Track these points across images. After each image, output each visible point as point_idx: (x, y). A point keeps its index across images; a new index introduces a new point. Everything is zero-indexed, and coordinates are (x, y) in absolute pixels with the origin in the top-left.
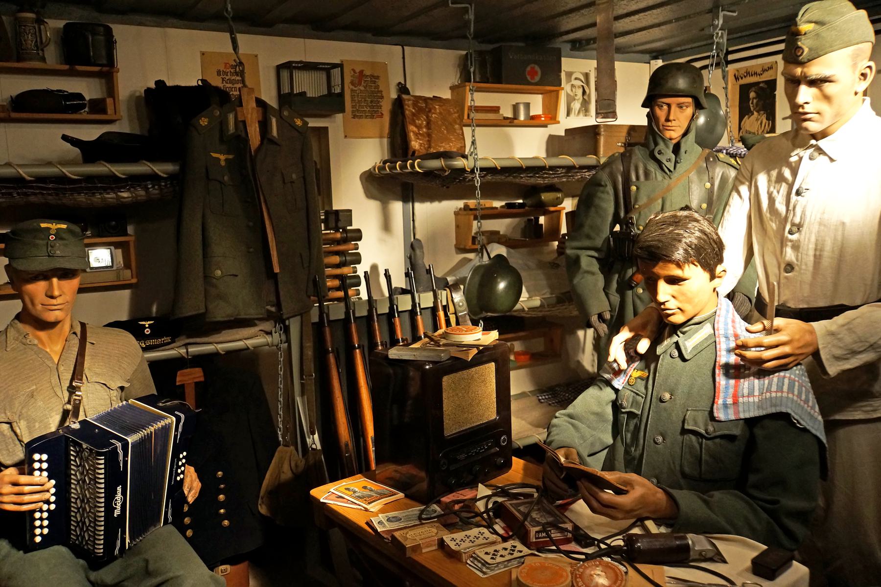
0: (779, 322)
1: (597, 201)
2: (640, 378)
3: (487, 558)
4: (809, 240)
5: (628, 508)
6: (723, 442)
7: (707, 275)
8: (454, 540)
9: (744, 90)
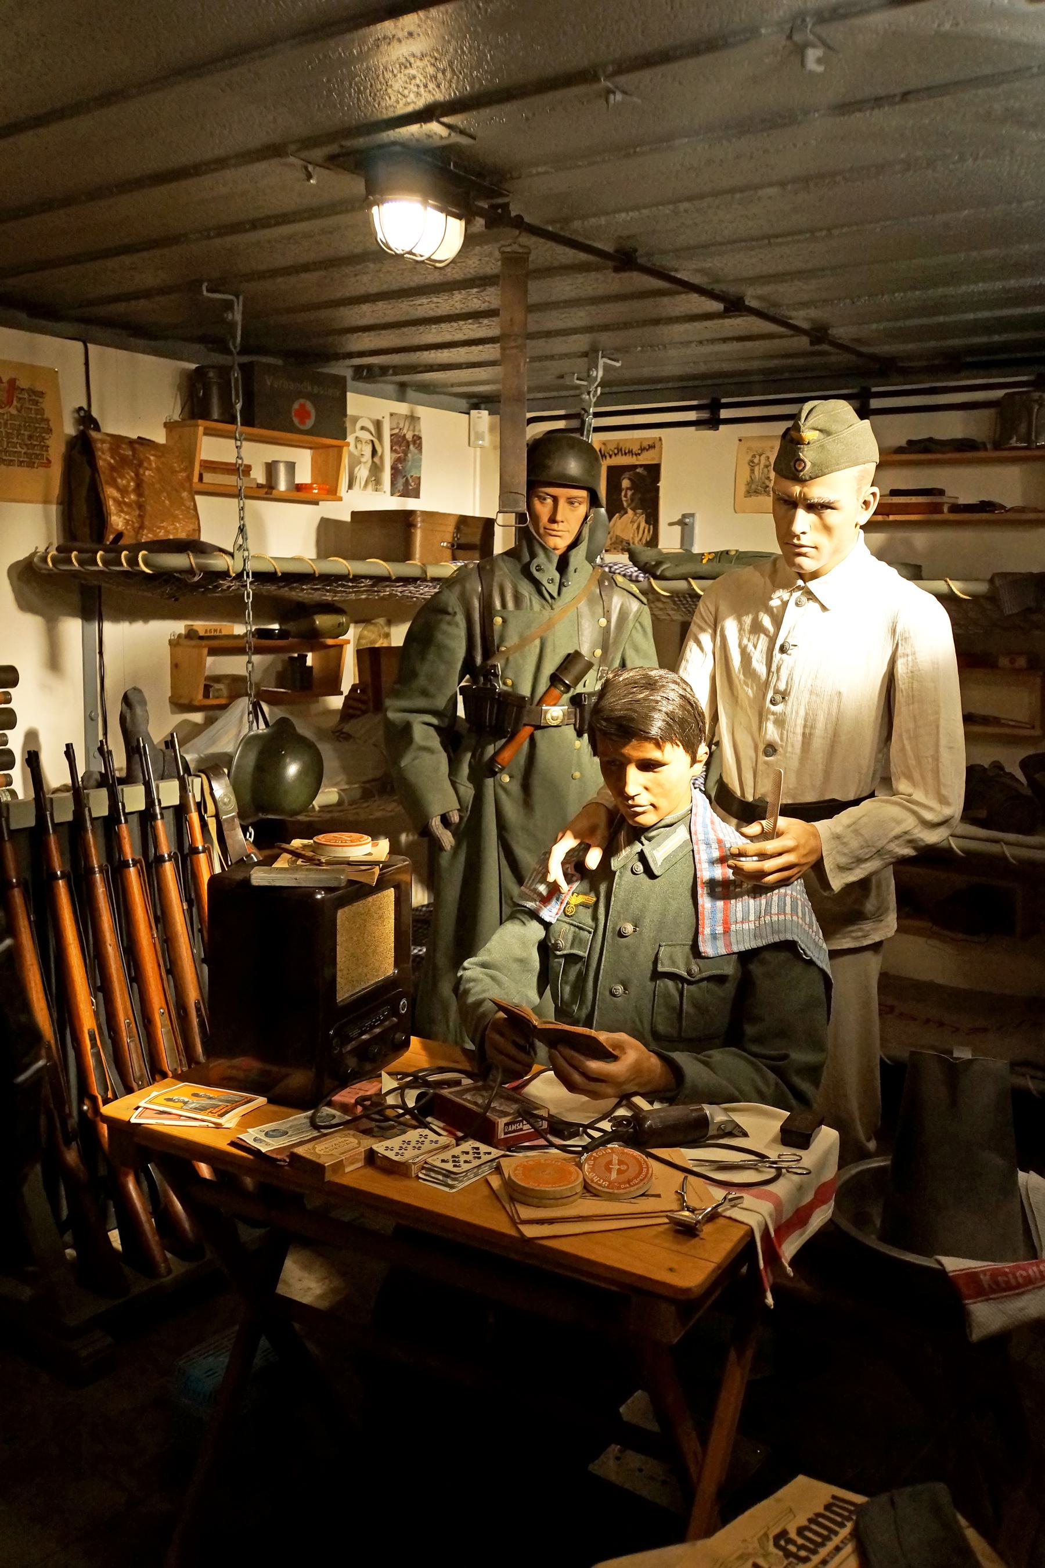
0: (783, 822)
1: (440, 637)
2: (585, 905)
3: (449, 1166)
4: (797, 713)
5: (622, 1079)
6: (712, 986)
7: (687, 759)
8: (388, 1148)
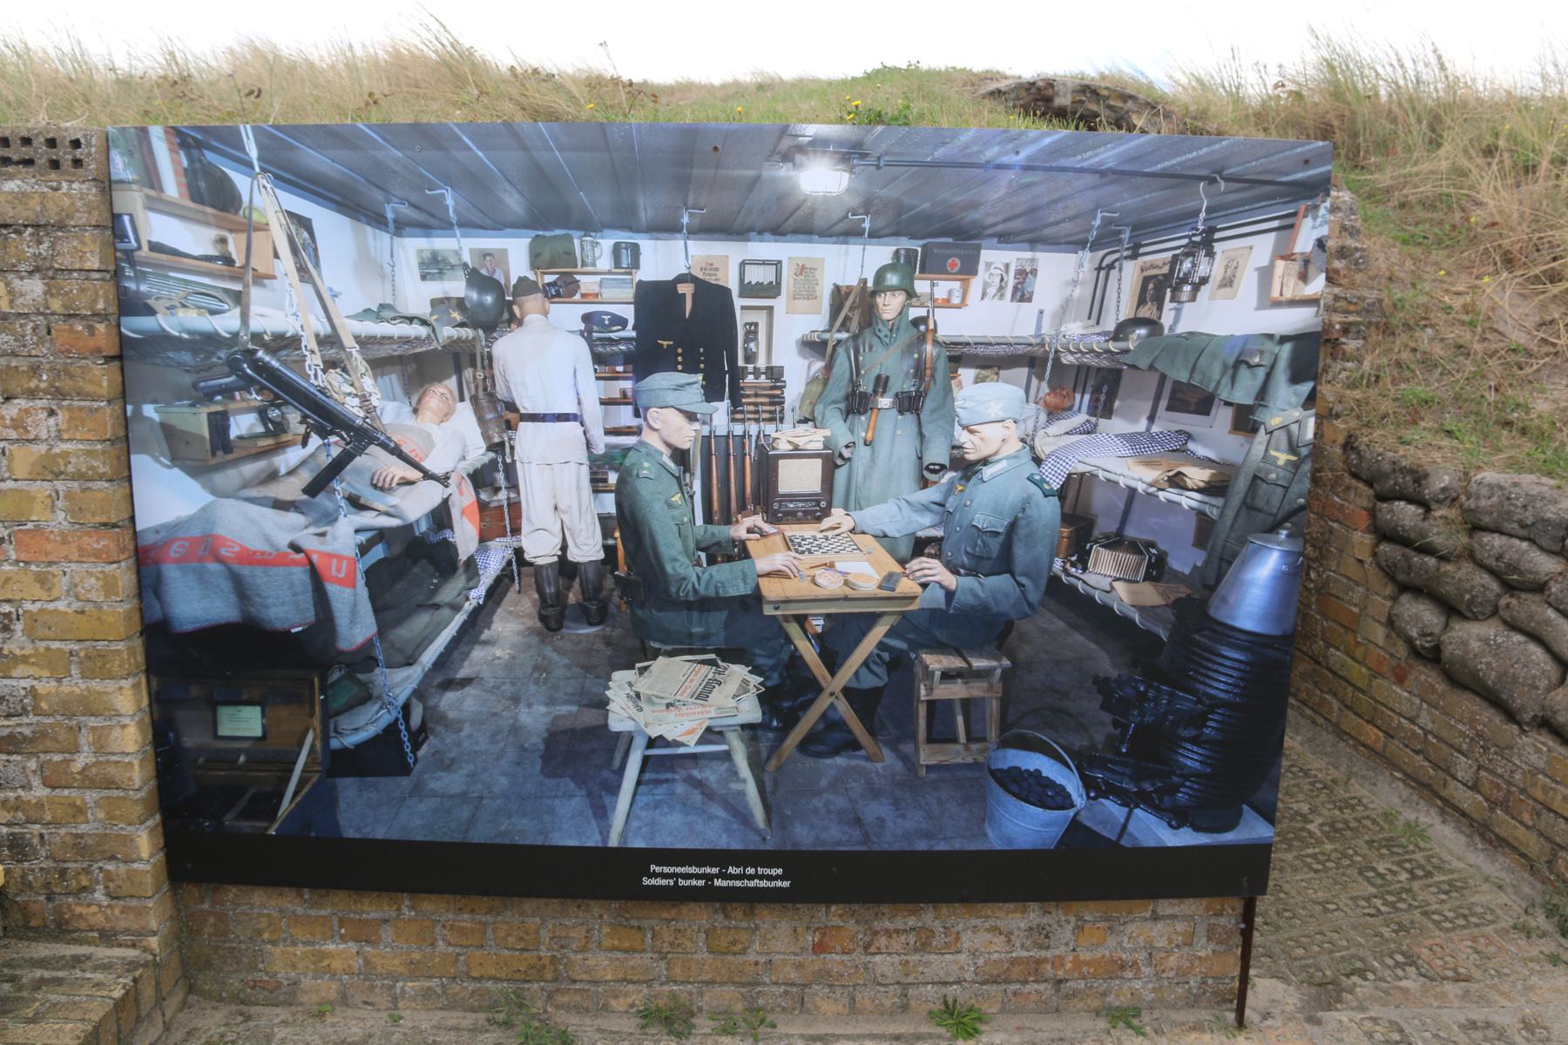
9: (1146, 280)
